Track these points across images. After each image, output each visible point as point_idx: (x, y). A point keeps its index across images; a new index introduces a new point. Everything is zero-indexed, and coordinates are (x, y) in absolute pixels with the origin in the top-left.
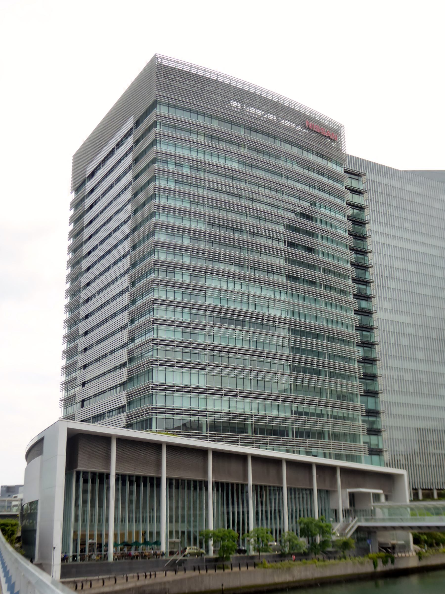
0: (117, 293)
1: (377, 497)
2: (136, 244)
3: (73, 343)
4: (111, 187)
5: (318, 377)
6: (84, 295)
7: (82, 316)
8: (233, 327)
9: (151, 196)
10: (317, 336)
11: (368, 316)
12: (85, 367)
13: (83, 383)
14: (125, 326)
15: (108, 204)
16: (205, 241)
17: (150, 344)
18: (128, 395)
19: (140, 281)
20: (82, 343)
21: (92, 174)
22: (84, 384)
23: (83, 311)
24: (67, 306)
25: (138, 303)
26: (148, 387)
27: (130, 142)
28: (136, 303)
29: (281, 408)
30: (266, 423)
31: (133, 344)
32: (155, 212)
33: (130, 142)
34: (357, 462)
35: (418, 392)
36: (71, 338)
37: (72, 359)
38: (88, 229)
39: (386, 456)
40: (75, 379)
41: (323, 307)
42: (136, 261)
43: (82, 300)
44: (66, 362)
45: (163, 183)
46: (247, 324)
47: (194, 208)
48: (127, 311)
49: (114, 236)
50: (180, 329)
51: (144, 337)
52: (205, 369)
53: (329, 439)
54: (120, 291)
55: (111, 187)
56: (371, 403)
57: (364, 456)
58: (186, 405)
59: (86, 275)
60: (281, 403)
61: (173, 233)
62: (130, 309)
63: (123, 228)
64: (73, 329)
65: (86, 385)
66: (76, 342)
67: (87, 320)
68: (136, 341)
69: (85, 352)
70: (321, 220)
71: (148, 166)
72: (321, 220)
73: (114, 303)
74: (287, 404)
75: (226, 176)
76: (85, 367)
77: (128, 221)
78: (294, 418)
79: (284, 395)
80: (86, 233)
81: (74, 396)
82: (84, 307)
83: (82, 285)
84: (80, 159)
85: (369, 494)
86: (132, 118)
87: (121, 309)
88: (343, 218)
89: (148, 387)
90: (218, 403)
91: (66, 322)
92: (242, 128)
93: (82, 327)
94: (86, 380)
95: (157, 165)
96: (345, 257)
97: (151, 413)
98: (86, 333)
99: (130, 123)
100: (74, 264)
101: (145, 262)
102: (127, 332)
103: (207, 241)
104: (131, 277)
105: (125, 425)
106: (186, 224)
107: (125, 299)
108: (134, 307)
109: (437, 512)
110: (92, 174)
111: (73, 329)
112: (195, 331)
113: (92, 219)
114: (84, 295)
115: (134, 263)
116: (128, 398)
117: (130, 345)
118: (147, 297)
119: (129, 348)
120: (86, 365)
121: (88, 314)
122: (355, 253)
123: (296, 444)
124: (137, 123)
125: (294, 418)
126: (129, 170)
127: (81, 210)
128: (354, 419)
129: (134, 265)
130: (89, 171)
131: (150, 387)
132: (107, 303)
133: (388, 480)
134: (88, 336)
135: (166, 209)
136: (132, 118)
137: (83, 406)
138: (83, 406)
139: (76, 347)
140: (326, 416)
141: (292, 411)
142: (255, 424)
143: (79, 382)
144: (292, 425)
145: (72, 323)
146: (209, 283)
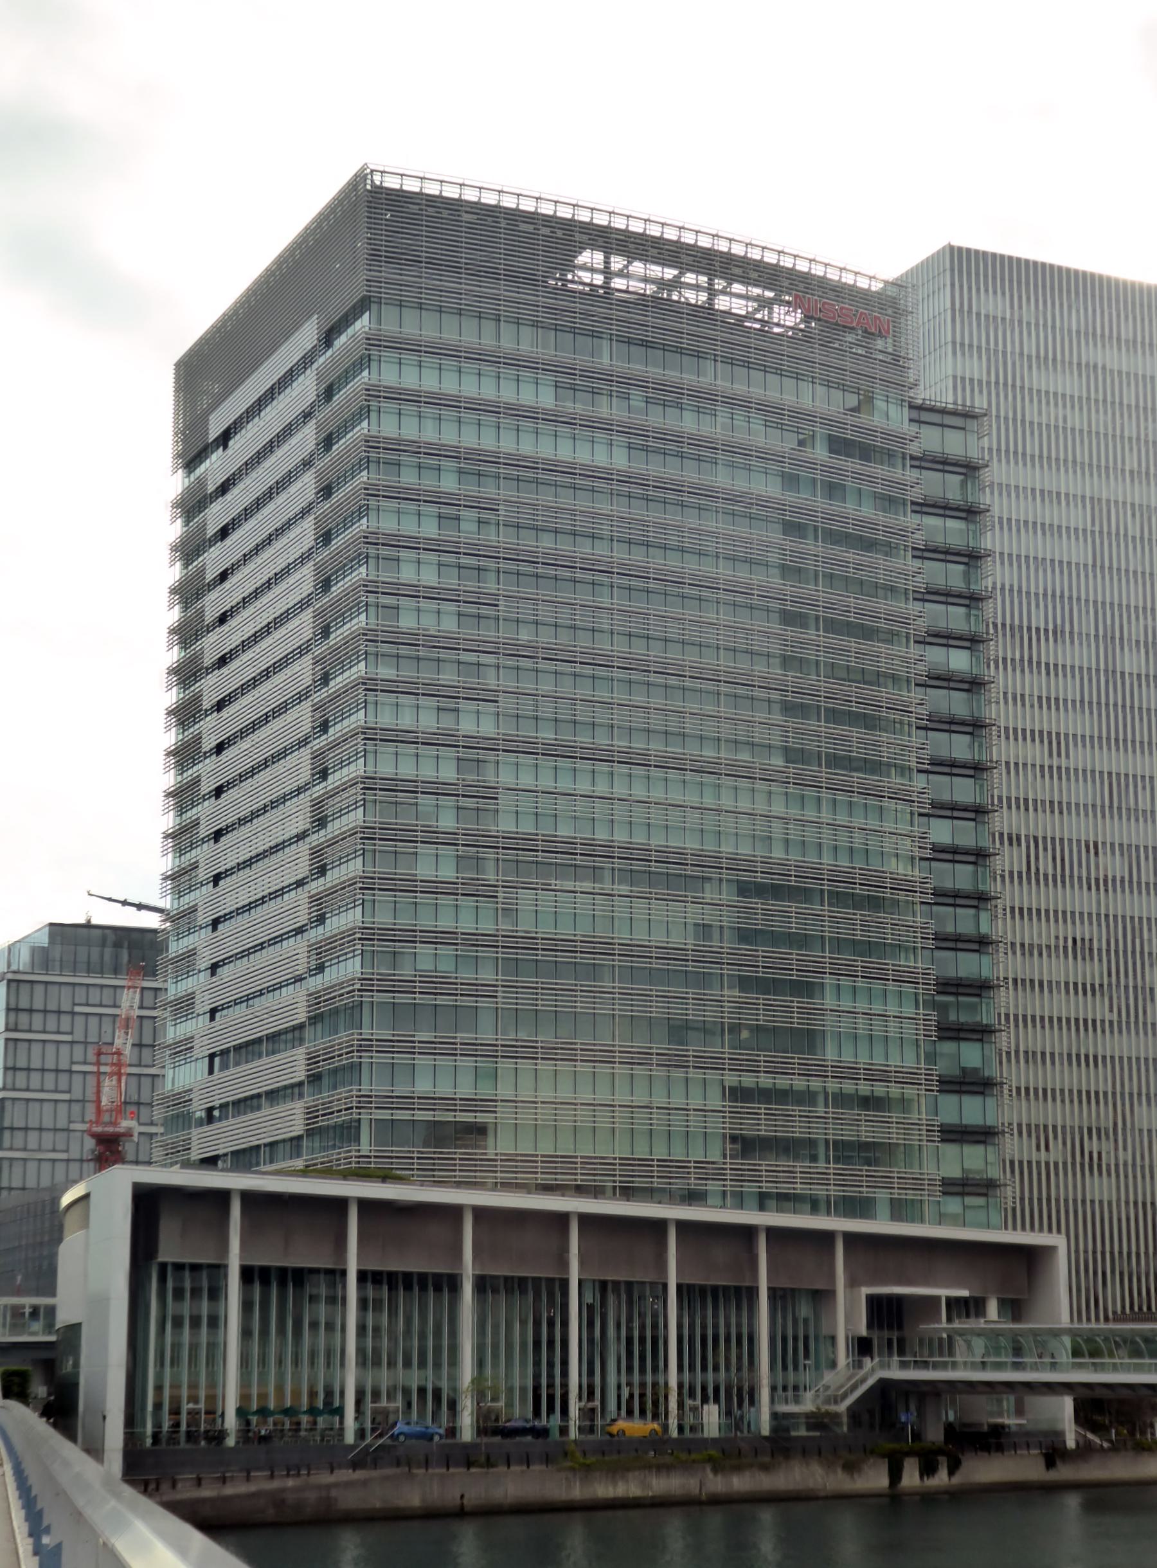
0: (289, 606)
1: (959, 1307)
3: (191, 730)
5: (798, 1002)
7: (210, 615)
8: (569, 885)
10: (802, 894)
12: (218, 835)
14: (303, 742)
18: (309, 1059)
20: (211, 729)
21: (224, 439)
22: (216, 879)
23: (213, 603)
30: (651, 1012)
31: (322, 833)
34: (907, 1221)
35: (1062, 457)
36: (185, 714)
37: (189, 814)
40: (195, 866)
41: (826, 816)
42: (330, 530)
43: (211, 531)
46: (607, 874)
48: (310, 656)
50: (432, 557)
51: (345, 771)
52: (496, 702)
53: (826, 1106)
54: (296, 601)
57: (930, 1198)
62: (317, 697)
65: (221, 883)
66: (197, 726)
68: (331, 731)
69: (219, 710)
73: (282, 631)
74: (712, 1076)
76: (218, 835)
79: (705, 1052)
81: (193, 910)
85: (937, 1299)
87: (299, 647)
90: (526, 1081)
92: (605, 342)
93: (211, 687)
94: (222, 869)
98: (220, 748)
105: (301, 1133)
106: (449, 436)
108: (324, 693)
109: (1148, 1369)
116: (309, 1065)
120: (221, 830)
121: (226, 612)
128: (904, 1103)
130: (214, 432)
132: (267, 630)
134: (225, 713)
135: (400, 397)
137: (212, 1019)
138: (212, 1019)
139: (198, 739)
142: (620, 967)
143: (203, 874)
145: (186, 674)
146: (506, 778)
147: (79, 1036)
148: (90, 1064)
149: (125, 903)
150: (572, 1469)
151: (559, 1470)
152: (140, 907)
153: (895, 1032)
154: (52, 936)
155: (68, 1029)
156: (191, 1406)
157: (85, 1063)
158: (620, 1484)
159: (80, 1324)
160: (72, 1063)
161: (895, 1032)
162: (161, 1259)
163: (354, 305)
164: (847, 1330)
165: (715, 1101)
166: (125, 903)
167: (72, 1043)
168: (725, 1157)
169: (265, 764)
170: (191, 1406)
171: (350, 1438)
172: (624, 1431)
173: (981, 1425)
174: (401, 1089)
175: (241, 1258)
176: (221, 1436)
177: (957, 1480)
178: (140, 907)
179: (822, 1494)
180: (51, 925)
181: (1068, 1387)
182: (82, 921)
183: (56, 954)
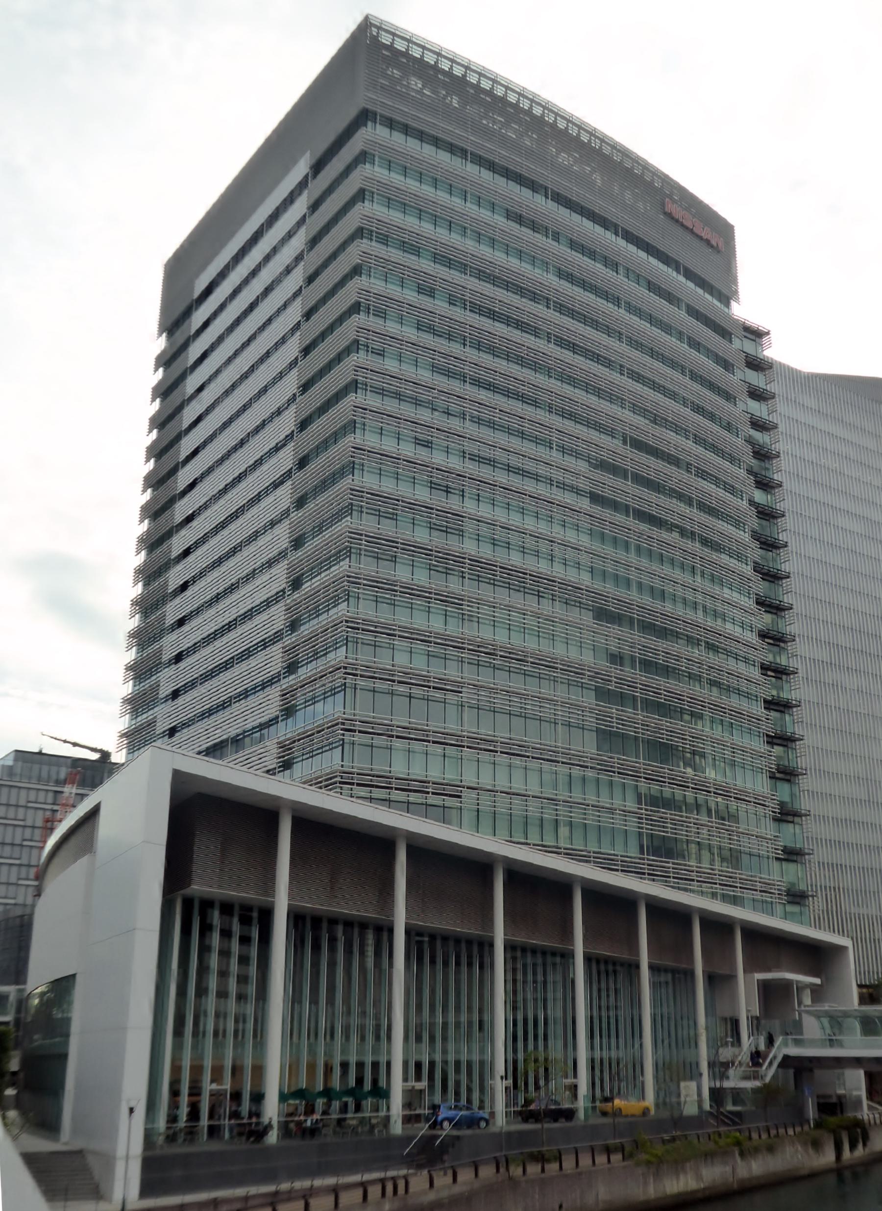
2: (306, 494)
4: (252, 307)
6: (173, 611)
9: (344, 427)
11: (754, 341)
13: (174, 691)
15: (238, 411)
16: (464, 577)
17: (340, 674)
19: (313, 538)
21: (208, 291)
24: (135, 603)
25: (307, 626)
26: (331, 779)
27: (300, 207)
28: (302, 628)
29: (617, 791)
32: (352, 504)
33: (300, 207)
38: (188, 467)
39: (817, 904)
44: (129, 723)
45: (371, 440)
47: (437, 583)
48: (279, 645)
49: (250, 479)
55: (252, 307)
56: (790, 835)
58: (417, 771)
59: (179, 567)
60: (616, 779)
61: (393, 514)
63: (270, 499)
64: (147, 684)
67: (182, 629)
70: (705, 607)
71: (340, 320)
72: (705, 607)
75: (509, 431)
77: (284, 445)
78: (643, 811)
80: (184, 477)
82: (173, 637)
83: (171, 589)
84: (178, 269)
86: (308, 154)
88: (747, 599)
89: (331, 779)
91: (129, 668)
95: (359, 358)
96: (753, 690)
97: (340, 783)
99: (302, 168)
100: (149, 576)
101: (327, 534)
102: (279, 693)
103: (467, 576)
104: (290, 569)
107: (277, 618)
110: (208, 291)
111: (147, 684)
112: (438, 695)
113: (196, 479)
114: (173, 611)
115: (301, 536)
117: (286, 680)
118: (331, 612)
119: (284, 687)
121: (183, 651)
122: (765, 611)
123: (649, 869)
124: (317, 167)
125: (643, 811)
126: (300, 194)
127: (169, 461)
129: (298, 543)
131: (336, 777)
133: (817, 956)
136: (308, 154)
140: (704, 810)
141: (639, 796)
144: (639, 828)
147: (24, 861)
148: (31, 880)
149: (65, 741)
150: (648, 1163)
151: (638, 1164)
152: (75, 744)
153: (593, 820)
154: (16, 760)
155: (18, 856)
156: (214, 1086)
157: (27, 879)
158: (682, 1177)
159: (74, 976)
160: (19, 879)
161: (593, 820)
162: (188, 891)
163: (154, 572)
164: (748, 1011)
165: (631, 804)
166: (65, 741)
167: (20, 865)
168: (642, 852)
169: (263, 425)
170: (214, 1086)
171: (397, 1128)
172: (620, 1109)
173: (830, 1097)
174: (380, 767)
175: (291, 896)
176: (258, 1133)
177: (867, 1150)
178: (75, 744)
179: (805, 1172)
180: (17, 751)
181: (857, 1062)
182: (37, 750)
183: (18, 770)
